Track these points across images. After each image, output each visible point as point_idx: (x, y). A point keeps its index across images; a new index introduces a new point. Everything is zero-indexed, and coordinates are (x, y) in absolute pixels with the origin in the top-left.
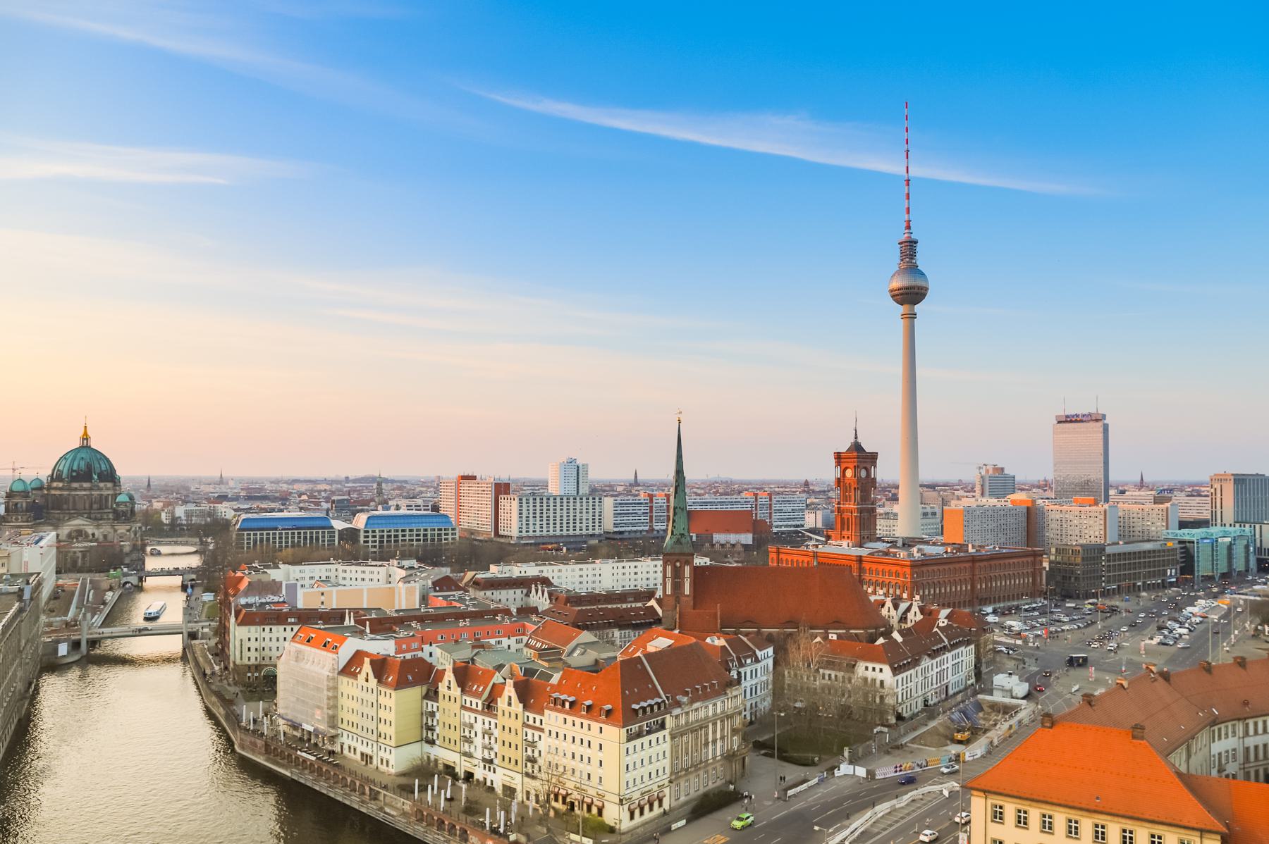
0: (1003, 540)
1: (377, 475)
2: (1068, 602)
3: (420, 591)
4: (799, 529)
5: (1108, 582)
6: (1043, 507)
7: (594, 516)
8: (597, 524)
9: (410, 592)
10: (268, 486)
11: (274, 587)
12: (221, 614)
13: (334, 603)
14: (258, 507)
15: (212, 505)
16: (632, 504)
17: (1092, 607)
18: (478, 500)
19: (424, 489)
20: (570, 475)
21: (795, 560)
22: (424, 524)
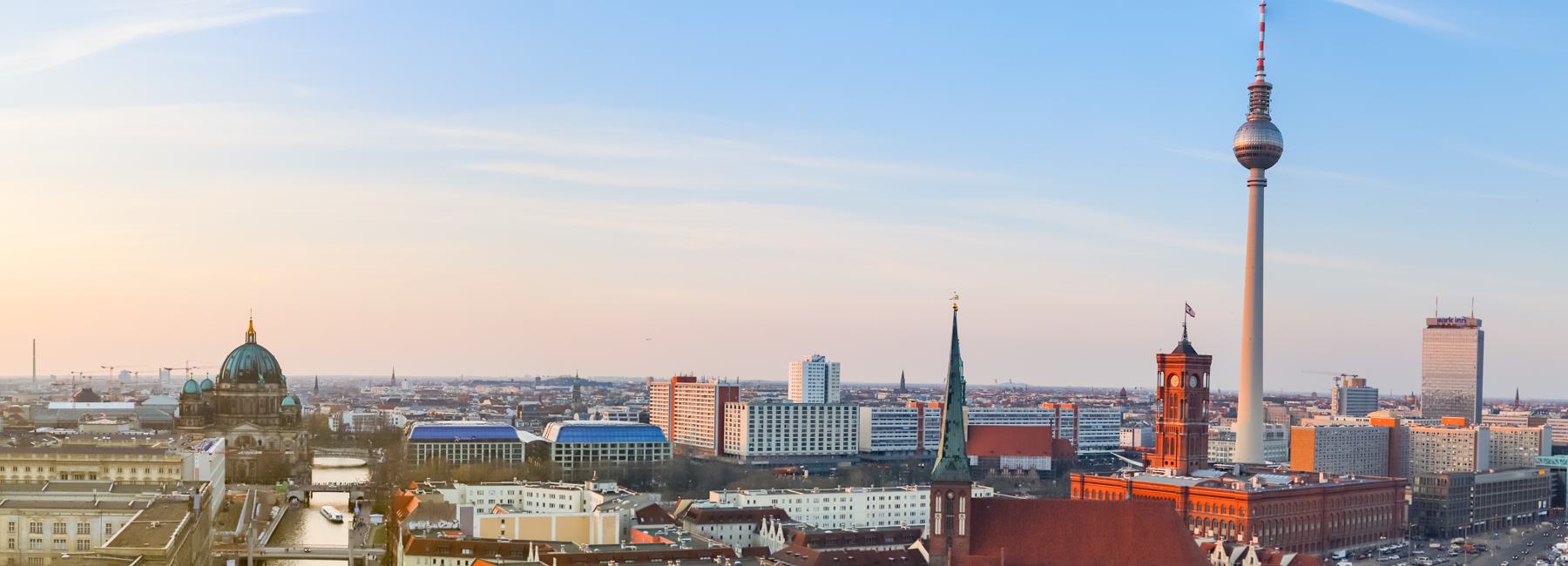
0: (1361, 468)
1: (574, 376)
2: (1432, 543)
3: (620, 523)
4: (1111, 452)
5: (1477, 517)
6: (1407, 428)
7: (846, 430)
8: (850, 441)
9: (608, 524)
10: (445, 388)
11: (447, 511)
12: (388, 539)
13: (516, 534)
14: (433, 413)
15: (382, 411)
16: (896, 415)
17: (1458, 547)
18: (698, 409)
19: (633, 394)
20: (816, 378)
21: (1097, 491)
22: (630, 438)
